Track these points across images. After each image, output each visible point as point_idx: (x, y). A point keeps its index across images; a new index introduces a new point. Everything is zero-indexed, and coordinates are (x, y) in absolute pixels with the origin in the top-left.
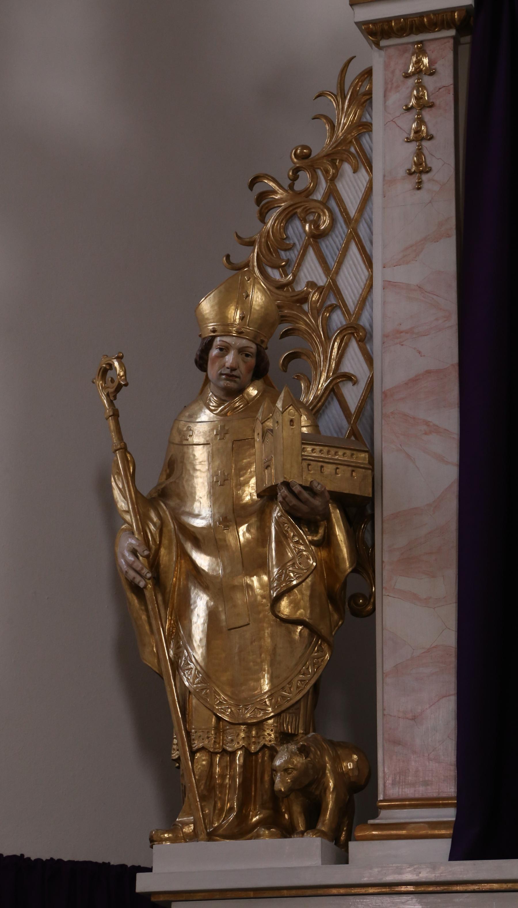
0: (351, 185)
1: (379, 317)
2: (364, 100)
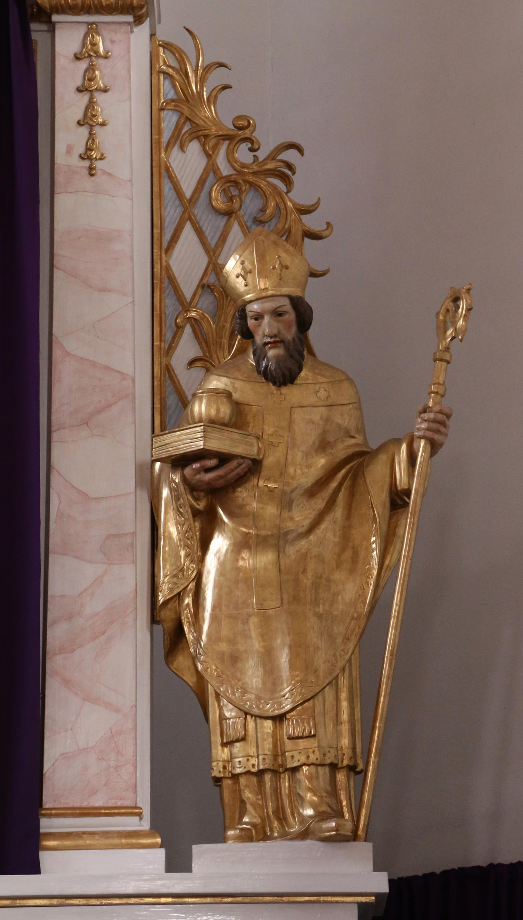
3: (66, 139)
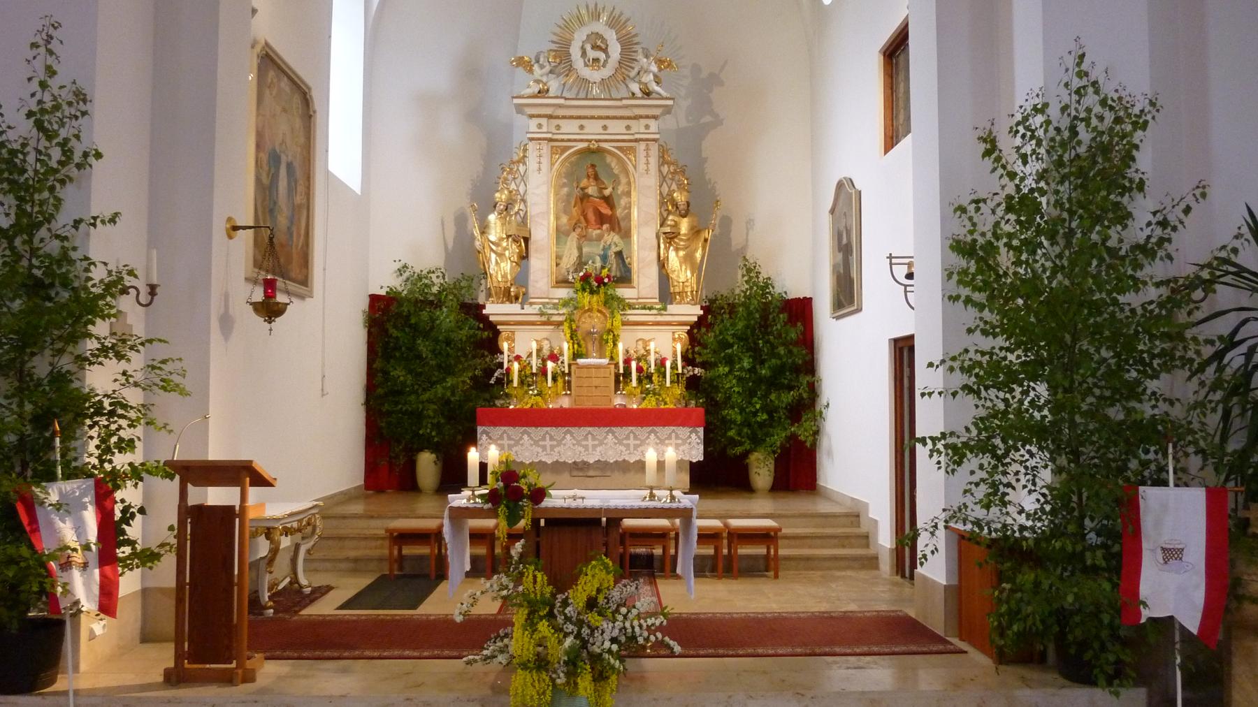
1: (529, 198)
2: (525, 150)
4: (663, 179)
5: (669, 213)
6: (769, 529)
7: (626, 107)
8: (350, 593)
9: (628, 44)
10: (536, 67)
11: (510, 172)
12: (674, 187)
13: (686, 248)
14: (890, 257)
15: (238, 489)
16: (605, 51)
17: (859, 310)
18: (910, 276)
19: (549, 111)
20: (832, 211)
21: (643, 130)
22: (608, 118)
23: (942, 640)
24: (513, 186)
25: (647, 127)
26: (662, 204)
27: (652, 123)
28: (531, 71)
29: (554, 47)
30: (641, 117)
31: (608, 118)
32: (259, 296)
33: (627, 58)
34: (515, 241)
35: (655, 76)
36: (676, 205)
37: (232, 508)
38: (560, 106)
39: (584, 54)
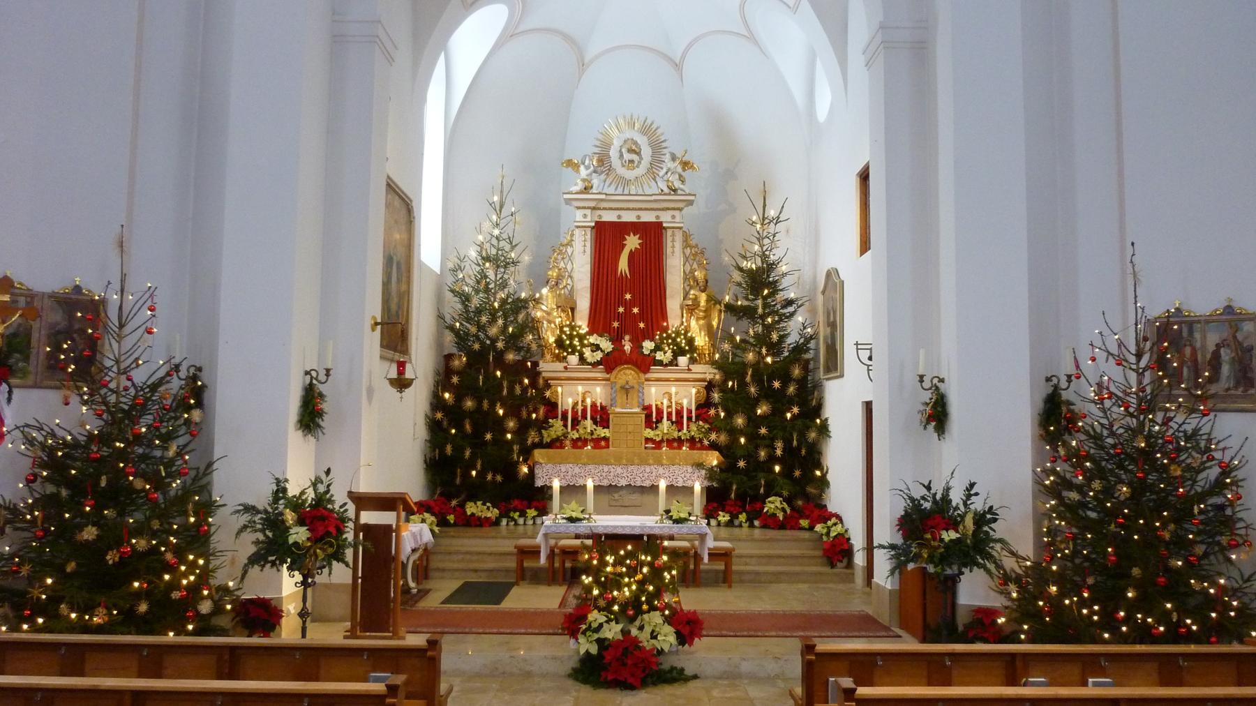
0: (569, 250)
1: (575, 275)
2: (572, 235)
3: (669, 250)
4: (686, 259)
5: (691, 288)
6: (727, 549)
7: (656, 201)
8: (447, 594)
9: (657, 147)
10: (582, 168)
11: (560, 253)
12: (695, 266)
13: (704, 318)
14: (857, 344)
15: (394, 513)
16: (638, 154)
17: (842, 376)
18: (870, 358)
19: (592, 204)
20: (823, 293)
21: (670, 219)
22: (640, 209)
23: (887, 629)
24: (562, 265)
25: (673, 217)
26: (685, 279)
27: (676, 213)
28: (578, 171)
29: (597, 150)
30: (668, 209)
31: (640, 209)
32: (393, 374)
33: (656, 161)
34: (563, 311)
35: (680, 176)
36: (696, 280)
37: (390, 526)
38: (602, 200)
39: (621, 156)
